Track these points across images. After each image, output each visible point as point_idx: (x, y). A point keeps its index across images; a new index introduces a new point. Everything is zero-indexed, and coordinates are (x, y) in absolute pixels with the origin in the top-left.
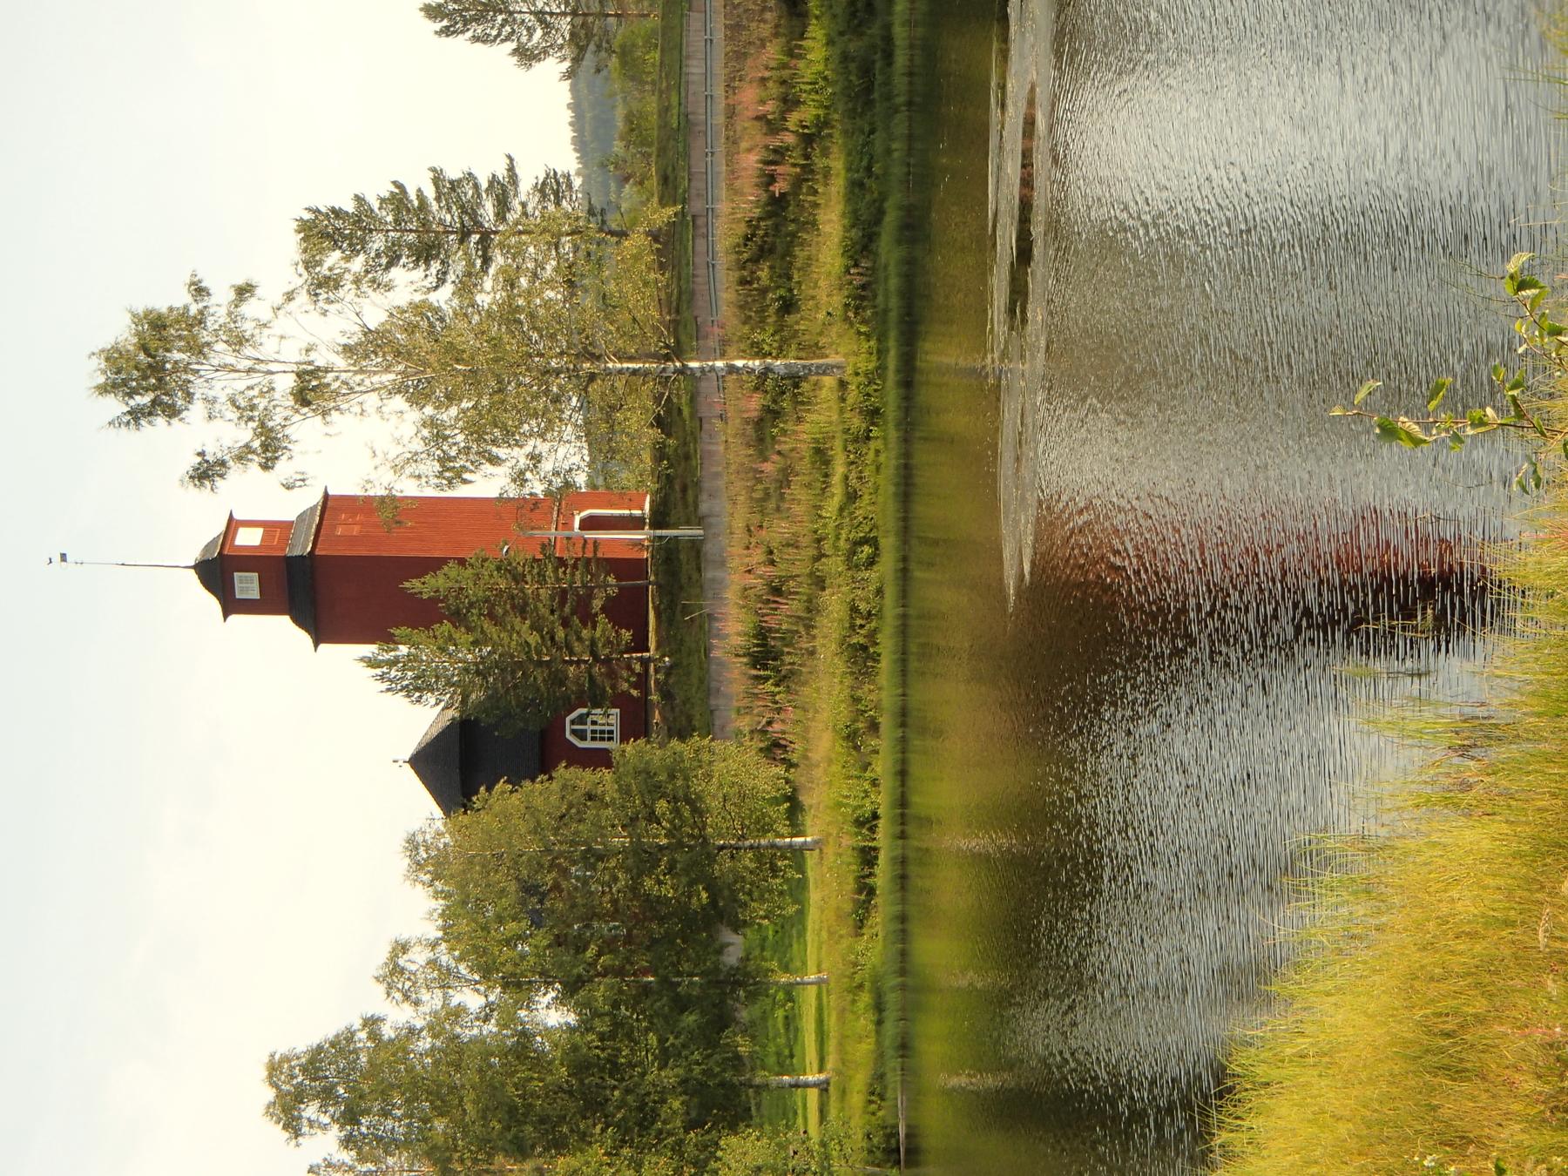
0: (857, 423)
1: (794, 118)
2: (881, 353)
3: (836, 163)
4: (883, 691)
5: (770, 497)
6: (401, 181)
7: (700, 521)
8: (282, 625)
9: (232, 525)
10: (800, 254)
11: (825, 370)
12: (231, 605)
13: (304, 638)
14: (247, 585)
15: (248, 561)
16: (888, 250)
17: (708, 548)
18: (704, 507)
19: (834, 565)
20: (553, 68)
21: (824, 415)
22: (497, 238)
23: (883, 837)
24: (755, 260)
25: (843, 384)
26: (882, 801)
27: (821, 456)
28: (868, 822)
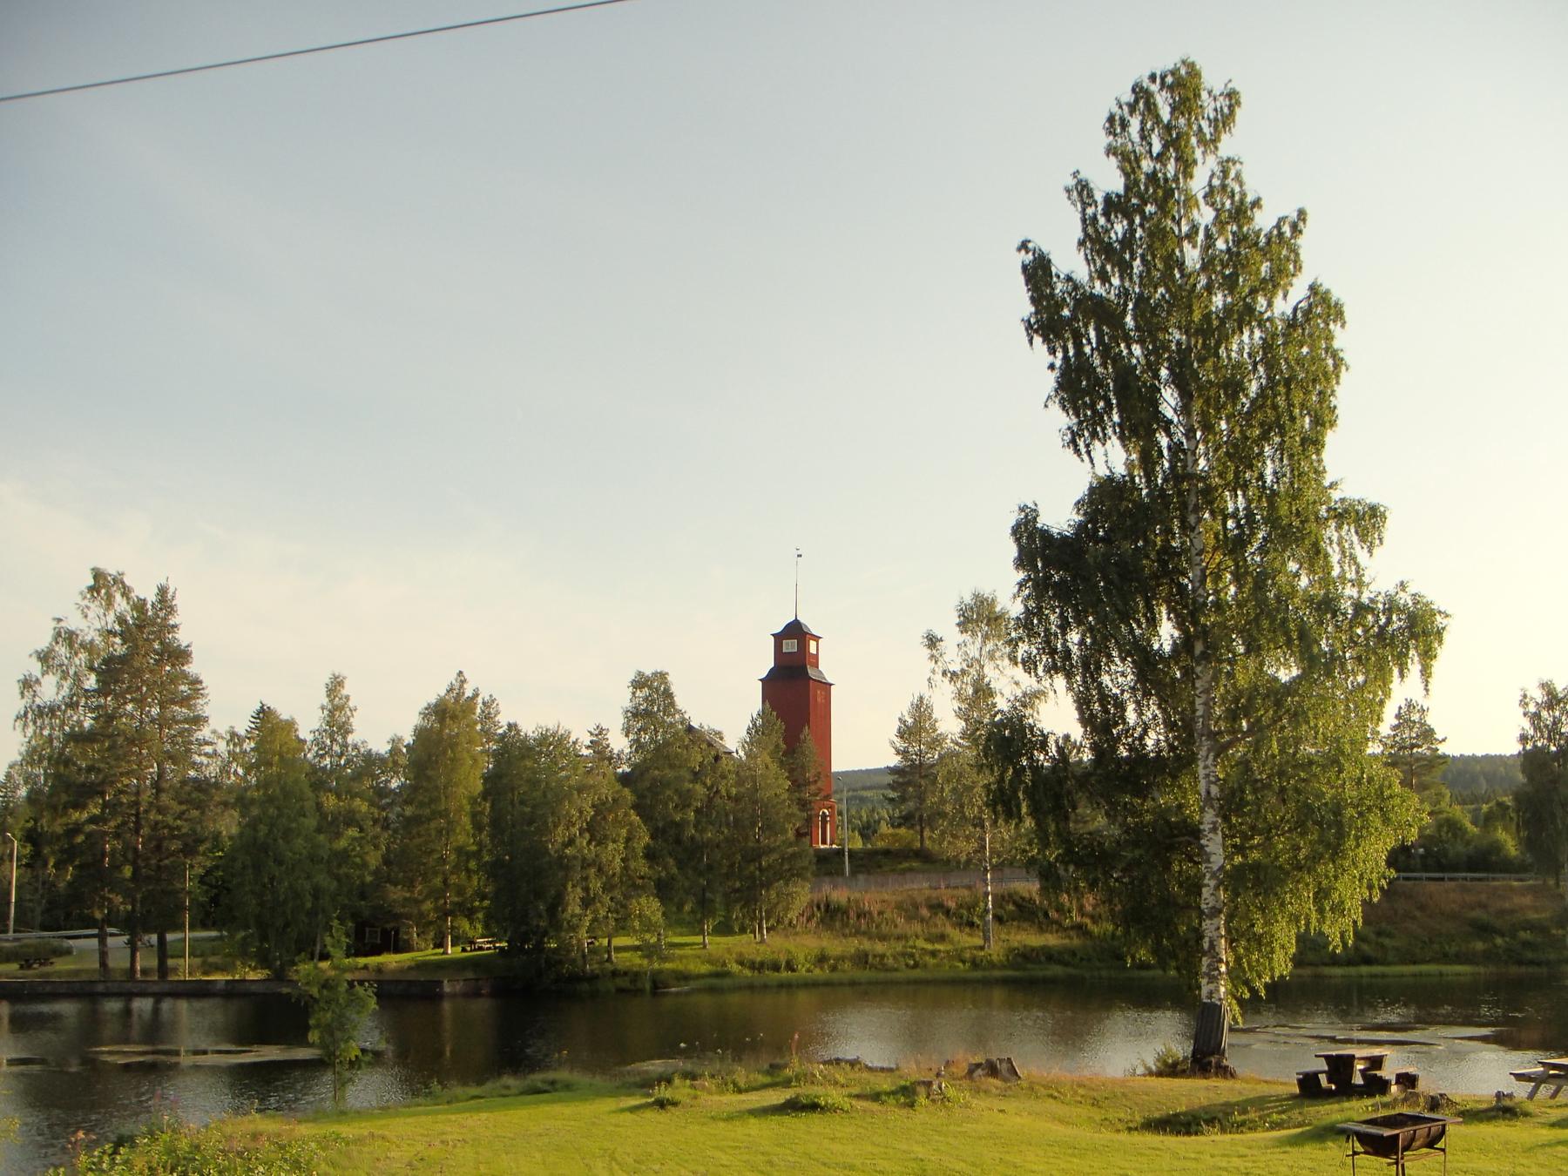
0: (967, 955)
1: (1087, 921)
2: (1003, 967)
3: (1076, 942)
4: (848, 971)
5: (910, 910)
6: (830, 663)
7: (854, 873)
8: (768, 663)
9: (817, 638)
10: (1025, 925)
11: (986, 939)
12: (779, 638)
13: (764, 675)
14: (790, 646)
15: (803, 646)
16: (1056, 970)
17: (840, 880)
18: (861, 877)
19: (899, 947)
20: (894, 760)
21: (967, 940)
22: (1551, 882)
23: (785, 975)
24: (1015, 903)
25: (982, 948)
26: (802, 972)
27: (942, 938)
28: (790, 967)
